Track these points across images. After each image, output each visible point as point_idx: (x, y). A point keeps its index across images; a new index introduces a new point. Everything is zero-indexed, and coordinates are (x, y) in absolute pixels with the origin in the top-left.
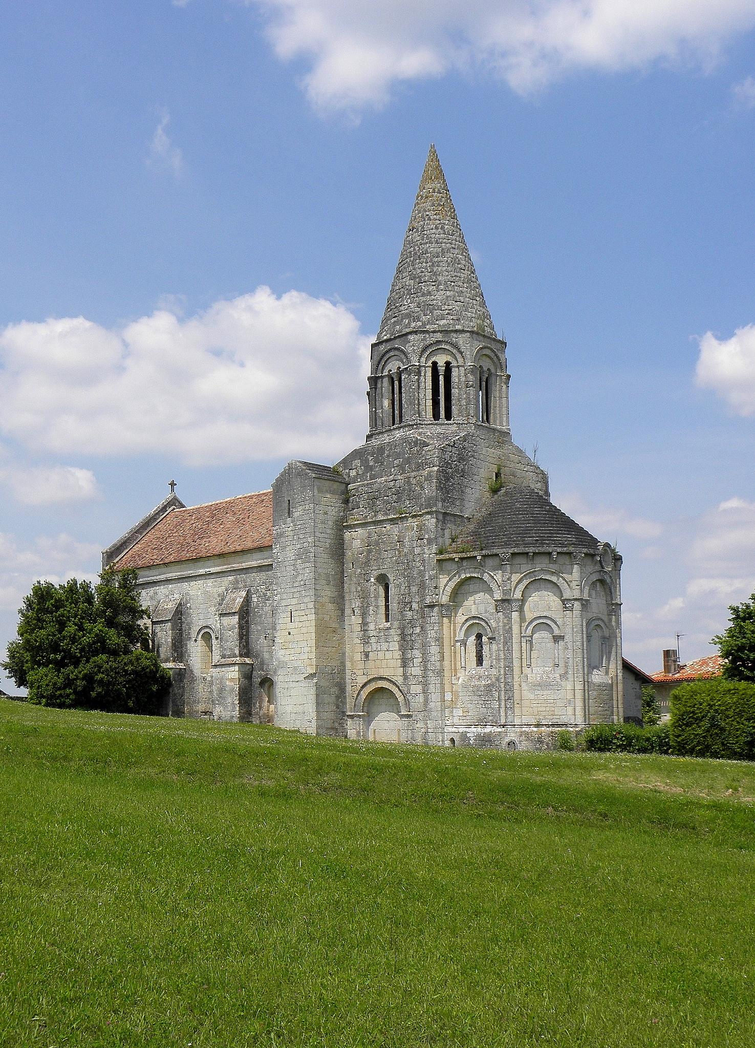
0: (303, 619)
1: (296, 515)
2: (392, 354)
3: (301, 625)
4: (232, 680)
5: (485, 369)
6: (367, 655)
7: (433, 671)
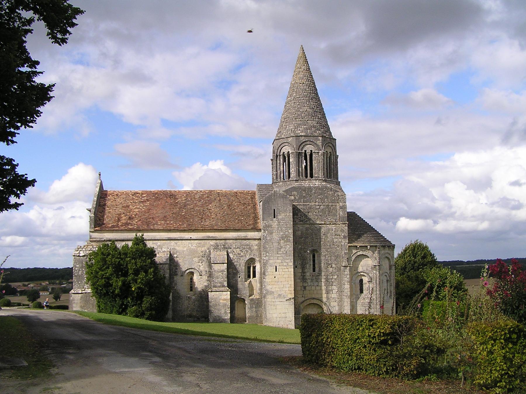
0: (284, 270)
1: (280, 217)
2: (308, 143)
3: (283, 273)
4: (225, 300)
5: (328, 152)
6: (305, 288)
7: (346, 296)
